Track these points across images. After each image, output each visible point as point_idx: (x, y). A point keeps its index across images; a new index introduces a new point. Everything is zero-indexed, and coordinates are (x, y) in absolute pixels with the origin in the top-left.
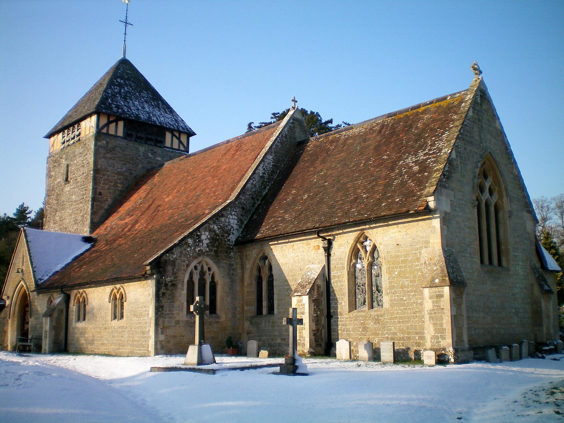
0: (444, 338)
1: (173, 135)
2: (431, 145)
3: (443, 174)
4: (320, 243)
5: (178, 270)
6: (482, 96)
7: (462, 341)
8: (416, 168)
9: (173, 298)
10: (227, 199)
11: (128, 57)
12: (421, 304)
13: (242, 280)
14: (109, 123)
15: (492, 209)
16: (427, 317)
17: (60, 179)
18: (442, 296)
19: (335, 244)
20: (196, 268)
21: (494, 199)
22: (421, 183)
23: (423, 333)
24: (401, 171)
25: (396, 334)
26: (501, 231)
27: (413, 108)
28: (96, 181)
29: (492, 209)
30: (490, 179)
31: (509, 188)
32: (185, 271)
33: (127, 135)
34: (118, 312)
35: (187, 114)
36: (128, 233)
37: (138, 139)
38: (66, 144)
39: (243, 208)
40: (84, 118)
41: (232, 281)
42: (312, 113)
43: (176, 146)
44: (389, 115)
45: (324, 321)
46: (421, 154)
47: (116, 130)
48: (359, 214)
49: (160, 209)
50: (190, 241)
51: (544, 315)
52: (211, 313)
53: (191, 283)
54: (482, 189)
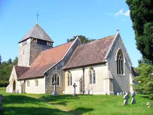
0: (108, 90)
1: (49, 42)
3: (109, 54)
6: (119, 36)
8: (103, 53)
9: (49, 81)
10: (62, 59)
14: (34, 40)
15: (121, 62)
17: (22, 53)
18: (107, 81)
21: (121, 59)
22: (104, 56)
23: (103, 89)
27: (104, 38)
28: (30, 54)
29: (121, 62)
35: (53, 39)
36: (39, 67)
37: (41, 44)
38: (23, 45)
40: (28, 39)
42: (84, 36)
43: (49, 45)
46: (105, 49)
47: (35, 42)
49: (46, 61)
50: (53, 69)
53: (53, 78)
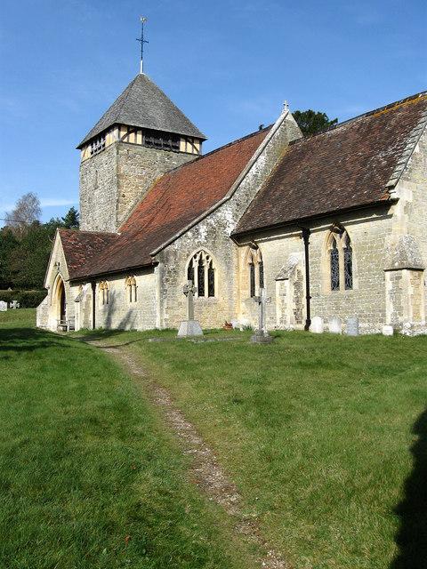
2: (400, 141)
5: (179, 259)
7: (419, 317)
13: (238, 267)
14: (127, 135)
16: (388, 296)
20: (195, 257)
24: (371, 167)
32: (186, 260)
33: (147, 144)
39: (238, 205)
42: (319, 114)
44: (368, 114)
48: (333, 206)
52: (199, 295)
53: (190, 270)
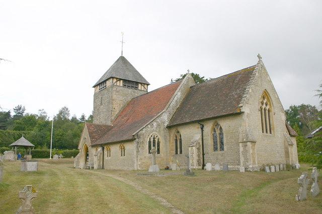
4: (200, 126)
11: (123, 56)
12: (239, 149)
19: (205, 127)
21: (268, 108)
25: (229, 161)
26: (271, 120)
30: (266, 99)
31: (274, 103)
34: (123, 154)
41: (166, 141)
45: (201, 156)
46: (238, 90)
51: (290, 153)
53: (150, 142)
54: (262, 103)
